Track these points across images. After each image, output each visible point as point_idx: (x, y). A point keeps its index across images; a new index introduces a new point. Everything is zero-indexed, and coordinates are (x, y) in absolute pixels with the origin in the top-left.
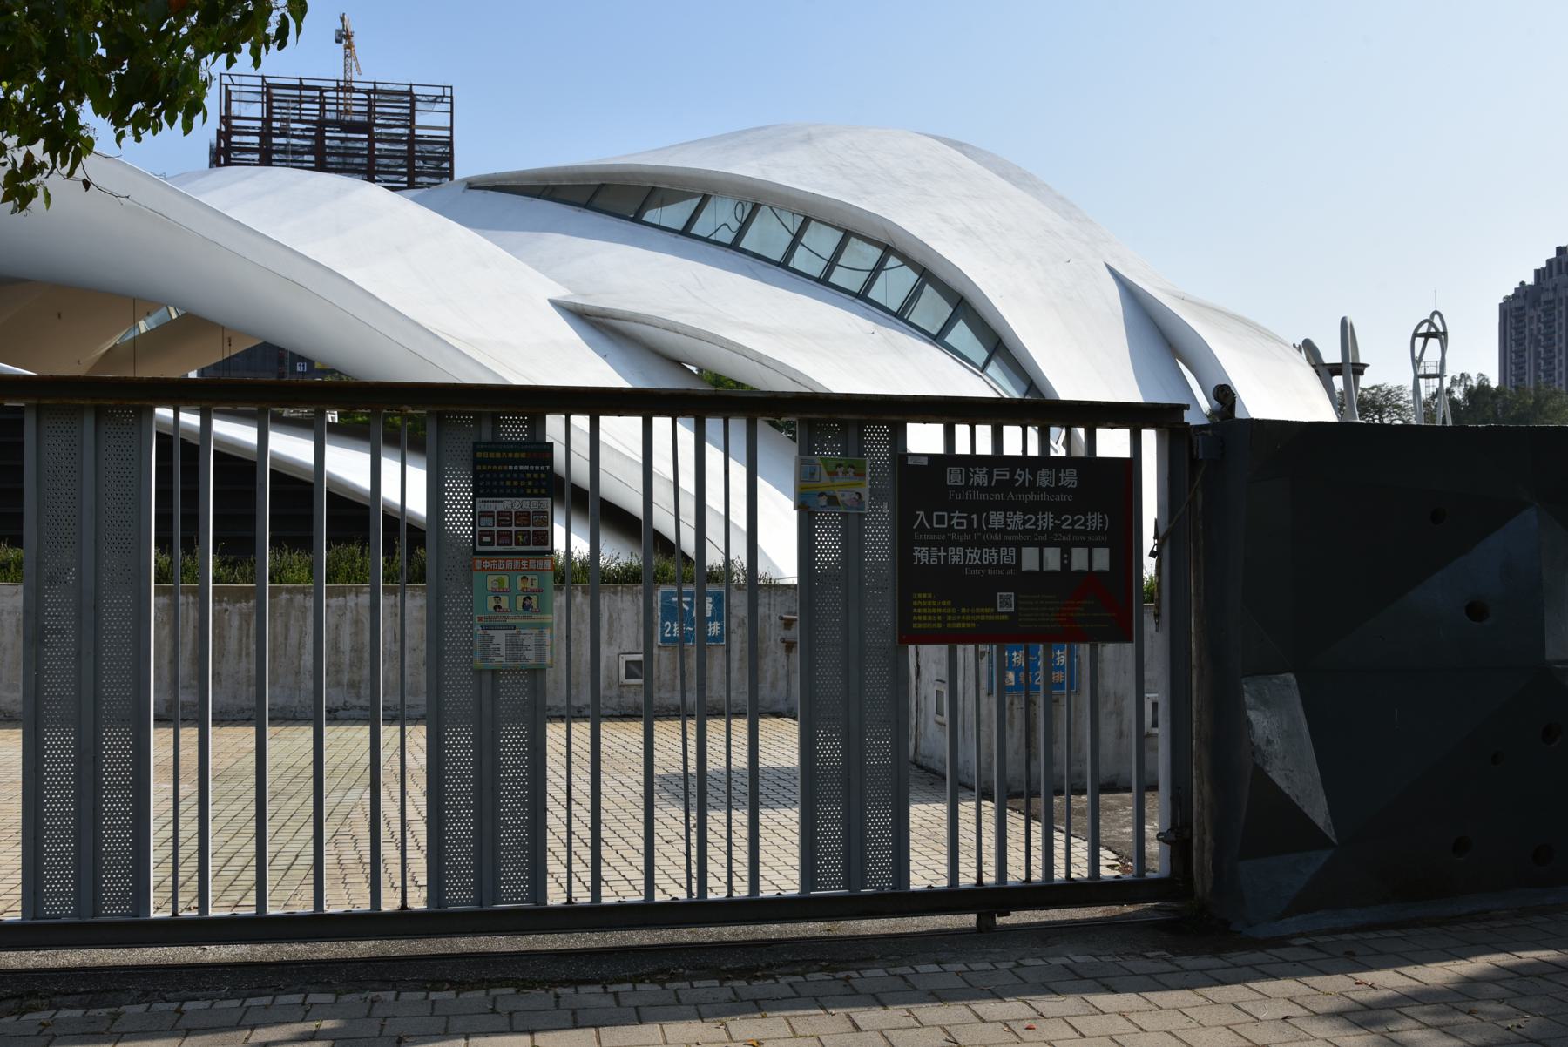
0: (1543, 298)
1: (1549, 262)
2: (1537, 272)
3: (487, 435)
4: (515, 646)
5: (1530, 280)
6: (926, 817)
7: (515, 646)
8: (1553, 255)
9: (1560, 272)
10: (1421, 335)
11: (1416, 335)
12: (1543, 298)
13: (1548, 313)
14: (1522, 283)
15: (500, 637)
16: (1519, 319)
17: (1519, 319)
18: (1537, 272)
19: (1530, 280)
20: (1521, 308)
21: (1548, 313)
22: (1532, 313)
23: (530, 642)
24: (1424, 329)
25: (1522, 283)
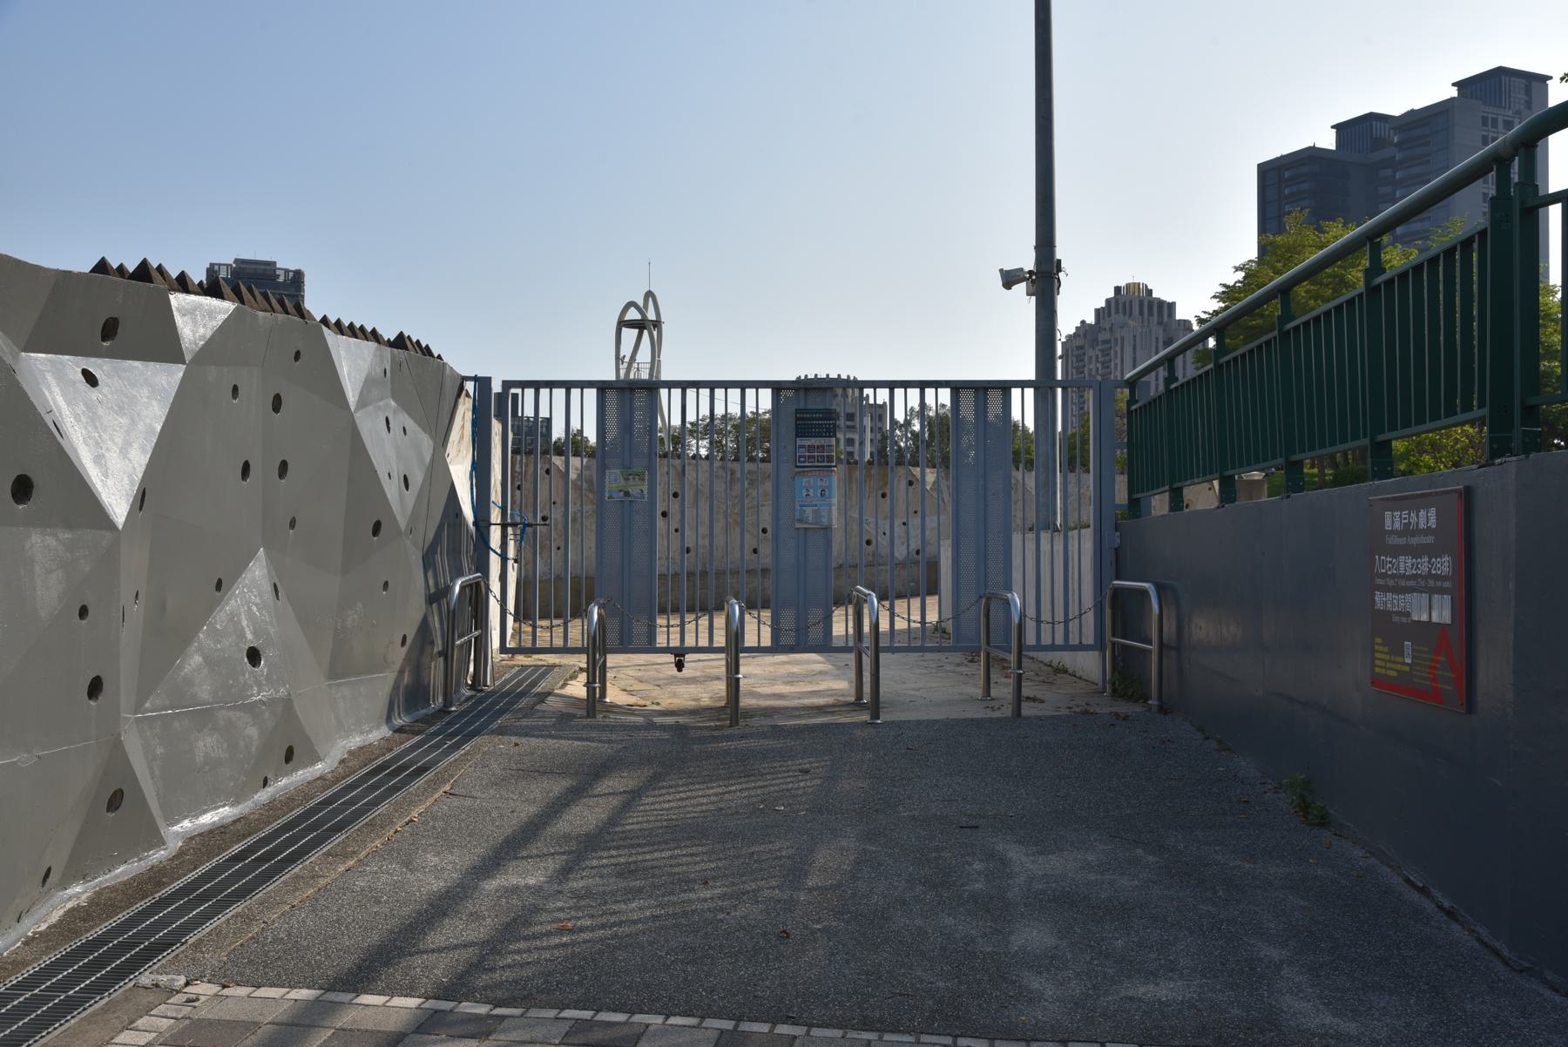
0: (1101, 337)
1: (1108, 301)
2: (1097, 311)
3: (802, 406)
4: (817, 514)
5: (1091, 320)
6: (1433, 523)
7: (817, 514)
8: (1112, 295)
9: (1117, 312)
10: (632, 324)
11: (623, 324)
12: (1101, 337)
13: (1106, 353)
14: (1083, 322)
15: (809, 510)
16: (1080, 359)
17: (1080, 359)
18: (1097, 311)
19: (1091, 320)
20: (1081, 347)
21: (1106, 353)
22: (1091, 352)
23: (824, 514)
24: (633, 315)
25: (1083, 322)
